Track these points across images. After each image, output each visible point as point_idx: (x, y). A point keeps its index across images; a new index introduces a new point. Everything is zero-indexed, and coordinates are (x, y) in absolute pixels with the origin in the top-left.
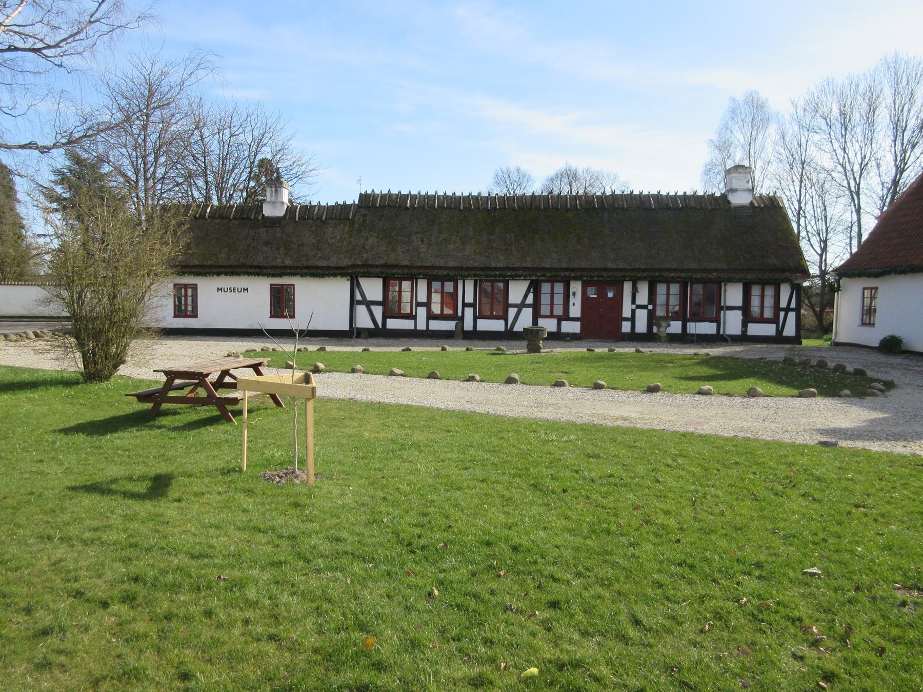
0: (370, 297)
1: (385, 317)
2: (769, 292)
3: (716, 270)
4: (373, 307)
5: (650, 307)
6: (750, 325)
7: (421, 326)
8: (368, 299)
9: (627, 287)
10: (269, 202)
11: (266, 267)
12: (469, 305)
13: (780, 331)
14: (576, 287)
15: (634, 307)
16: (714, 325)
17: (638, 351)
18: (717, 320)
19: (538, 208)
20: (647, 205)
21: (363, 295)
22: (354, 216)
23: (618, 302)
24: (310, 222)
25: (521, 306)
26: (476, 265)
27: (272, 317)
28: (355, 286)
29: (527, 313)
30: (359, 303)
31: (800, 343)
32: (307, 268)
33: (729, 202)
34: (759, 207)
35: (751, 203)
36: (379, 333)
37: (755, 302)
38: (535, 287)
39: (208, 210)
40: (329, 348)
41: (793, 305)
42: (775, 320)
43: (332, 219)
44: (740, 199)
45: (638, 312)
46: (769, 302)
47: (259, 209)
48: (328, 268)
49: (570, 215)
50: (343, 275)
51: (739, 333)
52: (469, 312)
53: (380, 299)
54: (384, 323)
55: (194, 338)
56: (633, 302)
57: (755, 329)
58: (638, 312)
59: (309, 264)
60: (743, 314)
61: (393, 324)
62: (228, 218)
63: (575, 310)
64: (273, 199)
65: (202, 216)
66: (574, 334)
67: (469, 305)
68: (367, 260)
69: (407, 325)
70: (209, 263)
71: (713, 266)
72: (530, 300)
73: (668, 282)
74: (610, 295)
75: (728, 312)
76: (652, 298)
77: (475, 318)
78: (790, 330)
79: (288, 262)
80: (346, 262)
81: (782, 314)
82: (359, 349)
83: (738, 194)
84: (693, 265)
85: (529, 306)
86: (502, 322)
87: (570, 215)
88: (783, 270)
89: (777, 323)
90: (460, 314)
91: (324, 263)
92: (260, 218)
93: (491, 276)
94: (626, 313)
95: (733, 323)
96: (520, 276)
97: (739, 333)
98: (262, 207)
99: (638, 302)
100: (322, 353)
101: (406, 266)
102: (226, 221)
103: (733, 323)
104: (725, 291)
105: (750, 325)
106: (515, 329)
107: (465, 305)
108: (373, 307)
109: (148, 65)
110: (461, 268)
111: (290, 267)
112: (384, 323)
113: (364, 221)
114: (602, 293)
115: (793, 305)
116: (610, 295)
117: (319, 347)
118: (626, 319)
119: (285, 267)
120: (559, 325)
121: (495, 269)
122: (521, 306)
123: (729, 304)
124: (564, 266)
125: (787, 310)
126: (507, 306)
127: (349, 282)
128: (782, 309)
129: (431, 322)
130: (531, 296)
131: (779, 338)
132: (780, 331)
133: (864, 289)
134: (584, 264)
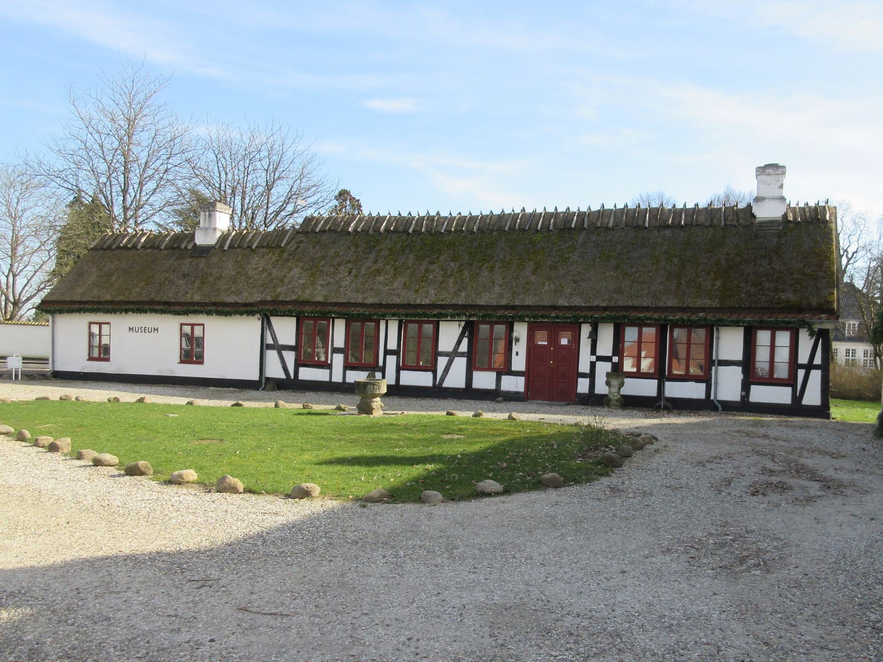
0: (282, 341)
1: (298, 364)
2: (783, 338)
3: (703, 309)
4: (284, 353)
5: (615, 359)
6: (754, 389)
7: (337, 378)
8: (280, 343)
9: (586, 330)
10: (201, 229)
11: (173, 304)
12: (392, 352)
13: (797, 398)
14: (521, 331)
15: (594, 358)
16: (703, 386)
17: (510, 418)
18: (706, 379)
19: (501, 230)
20: (640, 222)
21: (274, 338)
22: (288, 244)
23: (574, 351)
24: (239, 250)
25: (452, 355)
26: (398, 301)
27: (182, 362)
28: (266, 324)
29: (460, 364)
30: (269, 347)
31: (827, 416)
32: (215, 304)
33: (753, 216)
34: (795, 221)
35: (785, 216)
36: (289, 385)
37: (762, 355)
38: (470, 330)
39: (143, 240)
40: (246, 404)
41: (818, 360)
42: (790, 381)
43: (263, 247)
44: (766, 212)
45: (599, 364)
46: (783, 355)
47: (192, 237)
48: (236, 304)
49: (537, 237)
50: (250, 313)
51: (738, 398)
52: (392, 361)
53: (292, 342)
54: (296, 373)
55: (100, 384)
56: (593, 351)
57: (760, 394)
58: (599, 364)
59: (219, 299)
60: (744, 372)
61: (307, 374)
62: (158, 248)
63: (519, 362)
64: (207, 225)
65: (134, 247)
66: (517, 393)
67: (392, 352)
68: (278, 296)
69: (321, 375)
70: (120, 298)
71: (699, 303)
72: (464, 347)
73: (640, 324)
74: (564, 342)
75: (722, 369)
76: (618, 347)
77: (399, 369)
78: (812, 397)
79: (197, 298)
80: (256, 297)
81: (801, 373)
82: (228, 403)
83: (765, 205)
84: (672, 302)
85: (462, 355)
86: (430, 375)
87: (537, 237)
88: (800, 309)
89: (794, 386)
90: (381, 364)
91: (231, 299)
92: (190, 247)
93: (419, 315)
94: (584, 367)
95: (728, 384)
96: (446, 316)
97: (738, 398)
98: (194, 234)
99: (600, 352)
100: (141, 405)
101: (319, 303)
102: (155, 251)
103: (728, 384)
104: (718, 338)
105: (754, 389)
106: (445, 385)
107: (387, 352)
108: (284, 353)
109: (129, 84)
110: (380, 305)
111: (198, 304)
112: (296, 373)
113: (298, 247)
114: (553, 340)
115: (818, 360)
116: (564, 342)
117: (234, 402)
118: (584, 375)
119: (193, 304)
120: (498, 380)
121: (420, 306)
122: (452, 355)
123: (723, 357)
124: (504, 302)
125: (809, 367)
126: (436, 354)
127: (260, 322)
128: (802, 366)
129: (348, 372)
130: (465, 341)
131: (796, 408)
132: (797, 398)
133: (90, 323)
134: (529, 301)
